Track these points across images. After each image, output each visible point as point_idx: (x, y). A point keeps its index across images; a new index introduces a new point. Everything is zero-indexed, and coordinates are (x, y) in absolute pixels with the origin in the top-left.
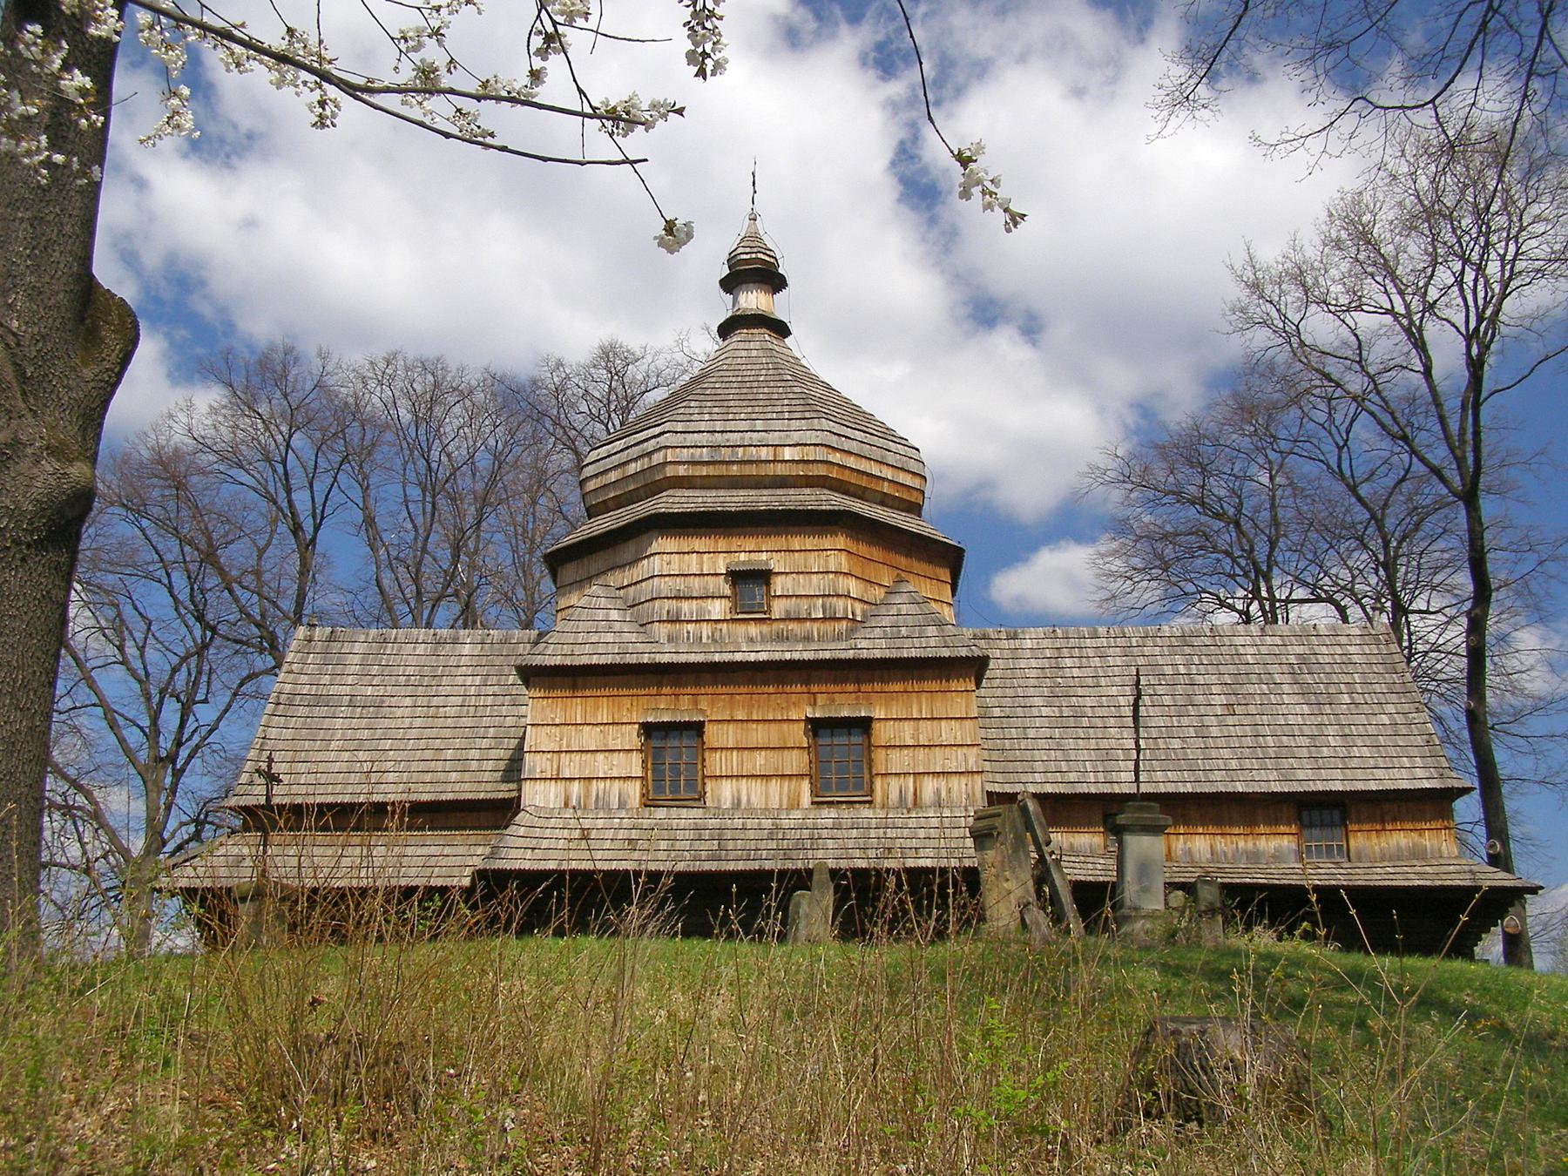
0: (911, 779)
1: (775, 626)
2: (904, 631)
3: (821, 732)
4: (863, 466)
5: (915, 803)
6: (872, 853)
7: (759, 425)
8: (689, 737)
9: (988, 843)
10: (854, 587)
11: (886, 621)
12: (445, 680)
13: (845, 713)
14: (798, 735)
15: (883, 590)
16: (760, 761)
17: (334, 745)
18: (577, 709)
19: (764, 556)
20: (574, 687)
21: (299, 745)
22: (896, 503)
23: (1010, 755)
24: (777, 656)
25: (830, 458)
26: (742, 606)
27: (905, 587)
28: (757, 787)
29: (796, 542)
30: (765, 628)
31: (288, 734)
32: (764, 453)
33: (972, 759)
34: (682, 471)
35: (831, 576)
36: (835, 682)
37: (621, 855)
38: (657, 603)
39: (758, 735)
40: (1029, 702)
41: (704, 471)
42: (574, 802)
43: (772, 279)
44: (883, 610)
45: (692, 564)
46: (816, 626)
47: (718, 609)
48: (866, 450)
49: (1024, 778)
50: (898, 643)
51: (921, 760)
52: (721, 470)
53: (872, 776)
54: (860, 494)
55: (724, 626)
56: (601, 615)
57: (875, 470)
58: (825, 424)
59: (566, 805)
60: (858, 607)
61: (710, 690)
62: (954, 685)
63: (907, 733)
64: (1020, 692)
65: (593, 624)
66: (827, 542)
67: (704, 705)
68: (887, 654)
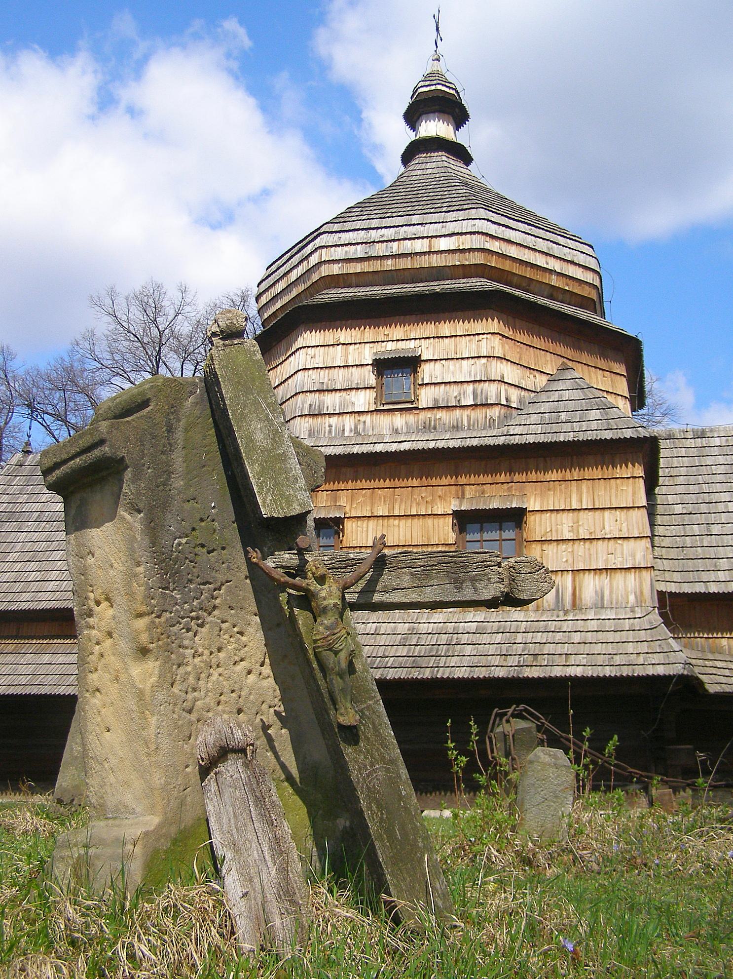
1: (423, 416)
3: (469, 526)
6: (513, 661)
7: (415, 219)
9: (98, 500)
10: (511, 374)
13: (494, 505)
15: (545, 378)
17: (11, 557)
19: (412, 344)
23: (691, 553)
24: (420, 446)
25: (488, 246)
27: (569, 374)
29: (446, 328)
30: (411, 418)
32: (420, 246)
33: (639, 553)
34: (336, 269)
35: (484, 361)
36: (486, 473)
38: (300, 397)
40: (714, 497)
41: (358, 268)
43: (457, 113)
44: (543, 397)
45: (337, 356)
46: (466, 413)
47: (363, 400)
48: (529, 241)
49: (705, 576)
50: (555, 428)
51: (581, 556)
52: (376, 266)
55: (367, 418)
57: (540, 261)
58: (482, 213)
60: (514, 394)
61: (350, 485)
62: (619, 472)
63: (564, 526)
64: (705, 488)
66: (478, 326)
67: (343, 502)
68: (542, 439)
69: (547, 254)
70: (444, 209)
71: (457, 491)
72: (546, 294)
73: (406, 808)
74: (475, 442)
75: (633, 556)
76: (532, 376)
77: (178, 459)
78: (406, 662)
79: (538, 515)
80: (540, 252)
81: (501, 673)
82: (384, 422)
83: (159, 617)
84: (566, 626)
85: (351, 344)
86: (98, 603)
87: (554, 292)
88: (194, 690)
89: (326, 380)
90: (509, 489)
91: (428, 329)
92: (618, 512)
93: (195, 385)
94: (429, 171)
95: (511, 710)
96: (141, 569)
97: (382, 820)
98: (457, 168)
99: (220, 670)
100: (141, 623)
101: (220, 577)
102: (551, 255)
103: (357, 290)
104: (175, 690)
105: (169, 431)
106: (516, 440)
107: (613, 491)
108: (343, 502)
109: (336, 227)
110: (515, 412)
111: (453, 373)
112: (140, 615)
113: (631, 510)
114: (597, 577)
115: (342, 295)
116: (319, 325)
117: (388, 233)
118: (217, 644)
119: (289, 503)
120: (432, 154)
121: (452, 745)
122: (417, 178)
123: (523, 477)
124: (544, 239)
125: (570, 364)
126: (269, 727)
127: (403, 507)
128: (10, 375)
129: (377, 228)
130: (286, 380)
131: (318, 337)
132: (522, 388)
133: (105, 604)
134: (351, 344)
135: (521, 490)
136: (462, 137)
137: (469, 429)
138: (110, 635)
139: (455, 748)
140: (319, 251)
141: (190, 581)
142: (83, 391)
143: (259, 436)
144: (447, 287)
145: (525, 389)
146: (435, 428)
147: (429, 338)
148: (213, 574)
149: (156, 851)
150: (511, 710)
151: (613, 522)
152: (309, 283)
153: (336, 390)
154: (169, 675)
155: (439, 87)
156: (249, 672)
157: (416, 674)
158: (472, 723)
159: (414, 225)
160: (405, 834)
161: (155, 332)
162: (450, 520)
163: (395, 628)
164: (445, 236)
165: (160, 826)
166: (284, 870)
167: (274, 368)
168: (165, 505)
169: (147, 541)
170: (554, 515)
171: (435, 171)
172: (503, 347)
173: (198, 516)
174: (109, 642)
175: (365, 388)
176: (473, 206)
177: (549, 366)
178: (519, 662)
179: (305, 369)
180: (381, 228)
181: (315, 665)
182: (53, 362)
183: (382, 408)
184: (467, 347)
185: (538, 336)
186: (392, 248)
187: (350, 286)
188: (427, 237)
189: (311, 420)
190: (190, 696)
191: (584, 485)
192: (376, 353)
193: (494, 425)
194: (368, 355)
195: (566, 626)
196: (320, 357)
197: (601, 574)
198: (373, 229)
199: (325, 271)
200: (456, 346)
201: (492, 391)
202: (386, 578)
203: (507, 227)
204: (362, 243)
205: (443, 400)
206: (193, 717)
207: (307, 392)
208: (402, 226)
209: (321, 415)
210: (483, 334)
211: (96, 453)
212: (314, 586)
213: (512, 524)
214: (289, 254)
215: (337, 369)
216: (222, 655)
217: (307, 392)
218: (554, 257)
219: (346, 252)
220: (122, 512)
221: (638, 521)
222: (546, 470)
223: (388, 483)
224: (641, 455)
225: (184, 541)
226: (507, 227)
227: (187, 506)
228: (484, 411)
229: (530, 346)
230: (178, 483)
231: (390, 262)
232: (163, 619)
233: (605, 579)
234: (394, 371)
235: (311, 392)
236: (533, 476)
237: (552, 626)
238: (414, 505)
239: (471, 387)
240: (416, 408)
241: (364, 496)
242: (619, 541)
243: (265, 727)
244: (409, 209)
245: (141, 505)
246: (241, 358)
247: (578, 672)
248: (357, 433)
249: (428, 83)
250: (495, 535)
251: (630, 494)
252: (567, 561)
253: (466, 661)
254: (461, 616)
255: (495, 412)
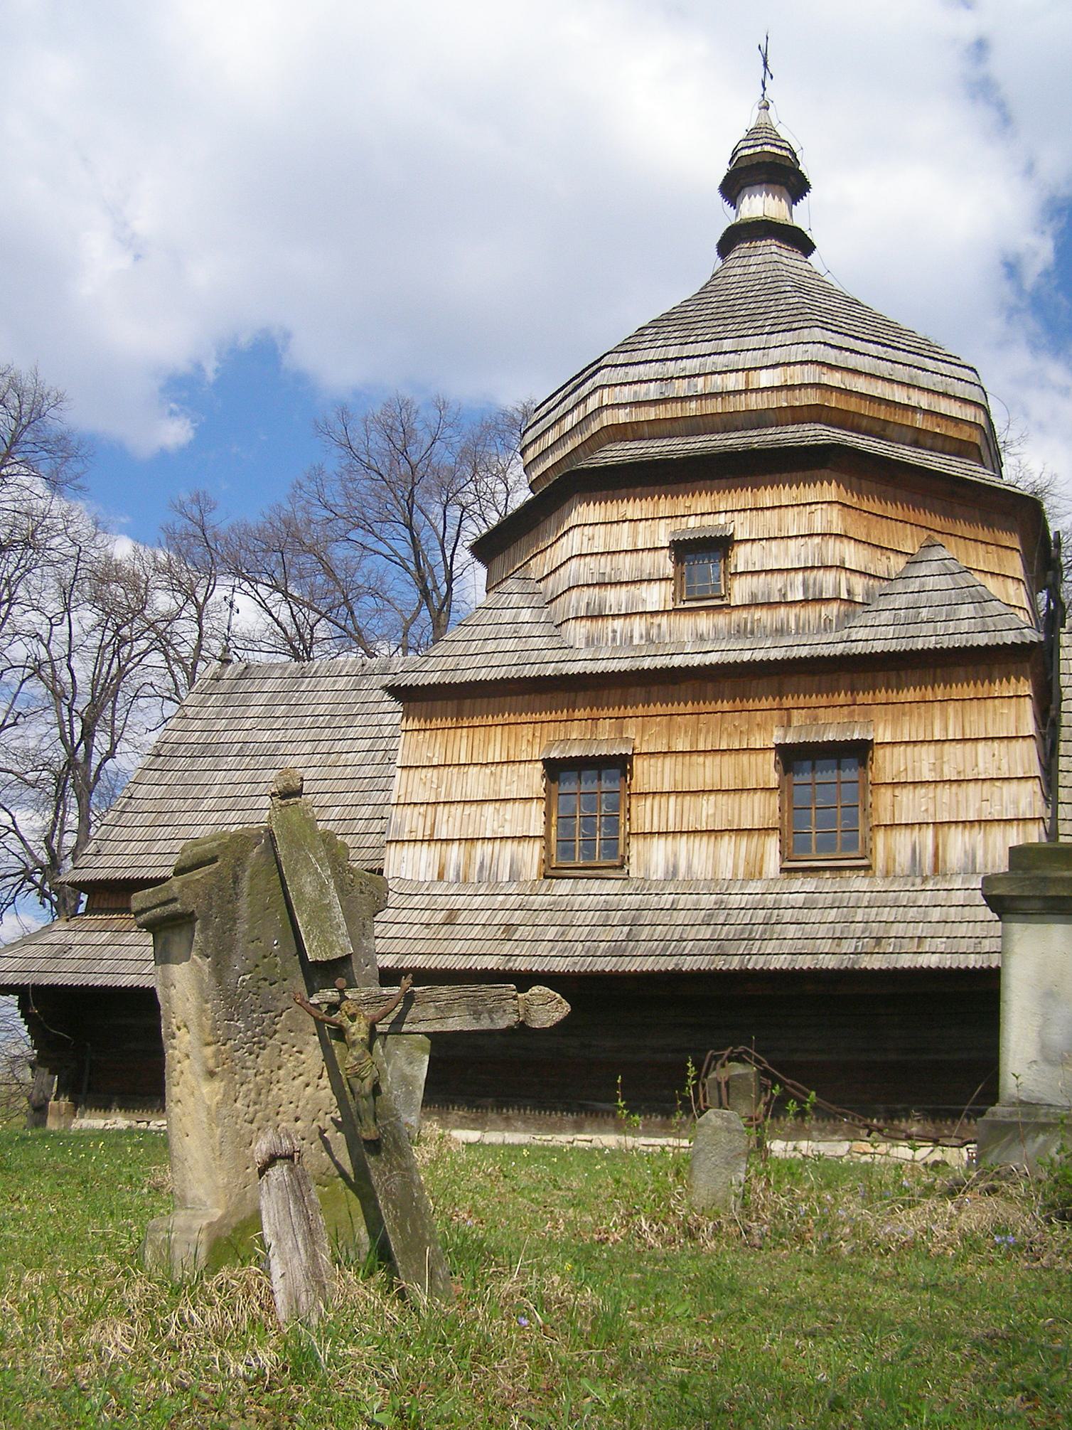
0: (930, 831)
1: (737, 616)
2: (924, 613)
4: (879, 389)
5: (936, 869)
6: (848, 946)
7: (727, 345)
8: (612, 780)
10: (853, 555)
11: (901, 601)
12: (359, 720)
13: (829, 737)
14: (767, 770)
15: (902, 561)
16: (707, 811)
17: (206, 804)
18: (461, 744)
19: (722, 519)
20: (459, 715)
21: (167, 805)
22: (939, 443)
24: (731, 657)
25: (825, 380)
26: (690, 590)
27: (937, 553)
28: (702, 846)
29: (767, 496)
30: (721, 620)
31: (158, 791)
32: (733, 382)
34: (622, 416)
35: (817, 540)
36: (819, 692)
37: (488, 946)
38: (575, 592)
39: (707, 772)
41: (651, 413)
42: (451, 875)
44: (899, 586)
45: (623, 536)
46: (794, 611)
47: (656, 596)
48: (884, 368)
50: (912, 629)
51: (946, 803)
52: (674, 411)
53: (546, 837)
54: (880, 430)
55: (663, 620)
56: (508, 615)
57: (899, 395)
58: (818, 334)
59: (441, 876)
60: (859, 584)
61: (640, 710)
62: (997, 689)
63: (924, 763)
65: (495, 630)
66: (809, 493)
67: (631, 732)
68: (893, 646)
69: (909, 386)
70: (767, 329)
71: (781, 718)
72: (908, 441)
73: (417, 1207)
74: (804, 652)
75: (1016, 803)
76: (884, 558)
77: (243, 906)
78: (709, 948)
79: (888, 749)
80: (899, 383)
81: (830, 963)
82: (685, 624)
83: (224, 1045)
84: (923, 899)
85: (641, 520)
86: (179, 1029)
87: (919, 439)
88: (255, 1103)
89: (608, 570)
90: (851, 714)
91: (744, 498)
92: (996, 744)
93: (261, 836)
94: (753, 269)
95: (727, 1053)
96: (209, 1006)
97: (396, 1217)
98: (791, 262)
99: (280, 1085)
100: (209, 1050)
101: (281, 1005)
102: (914, 387)
103: (650, 443)
104: (238, 1105)
105: (234, 882)
106: (859, 648)
107: (990, 715)
108: (631, 732)
109: (622, 358)
110: (859, 609)
111: (776, 557)
112: (208, 1044)
113: (1014, 741)
114: (967, 832)
115: (631, 452)
116: (599, 494)
117: (691, 366)
118: (277, 1064)
119: (332, 948)
120: (758, 243)
121: (621, 1104)
122: (735, 279)
123: (869, 698)
124: (904, 365)
125: (938, 538)
126: (325, 1131)
127: (709, 740)
128: (208, 533)
129: (677, 359)
130: (557, 569)
131: (597, 512)
132: (870, 575)
133: (184, 1030)
134: (641, 520)
135: (866, 715)
136: (802, 216)
137: (797, 633)
138: (187, 1056)
139: (625, 1107)
140: (600, 391)
141: (253, 1011)
142: (310, 550)
143: (308, 889)
144: (770, 438)
145: (875, 577)
146: (752, 632)
147: (744, 510)
148: (275, 1003)
149: (218, 1239)
150: (727, 1053)
151: (989, 756)
152: (587, 435)
153: (621, 583)
154: (232, 1093)
155: (767, 148)
156: (307, 1085)
157: (720, 964)
158: (689, 1065)
159: (726, 353)
160: (415, 1230)
161: (405, 468)
162: (772, 756)
163: (698, 901)
164: (767, 367)
165: (223, 1217)
166: (314, 1257)
167: (542, 552)
168: (229, 949)
169: (214, 981)
170: (910, 748)
171: (761, 268)
172: (844, 520)
173: (261, 954)
174: (187, 1061)
175: (660, 580)
176: (806, 324)
177: (909, 542)
178: (856, 947)
179: (581, 555)
180: (682, 358)
181: (347, 1089)
182: (267, 512)
183: (682, 606)
184: (794, 522)
185: (894, 502)
186: (696, 386)
187: (641, 439)
188: (743, 370)
189: (589, 623)
190: (251, 1109)
191: (951, 708)
192: (674, 533)
193: (831, 628)
194: (663, 534)
195: (923, 899)
196: (601, 539)
197: (972, 827)
198: (671, 359)
199: (608, 418)
200: (780, 520)
201: (828, 582)
202: (414, 1011)
203: (852, 351)
204: (656, 380)
205: (763, 594)
206: (254, 1126)
207: (583, 586)
208: (709, 355)
209: (602, 616)
210: (817, 503)
211: (171, 908)
212: (347, 1023)
213: (854, 761)
214: (561, 394)
215: (622, 555)
216: (281, 1072)
217: (583, 586)
218: (920, 388)
219: (635, 392)
220: (194, 956)
221: (1025, 757)
222: (899, 688)
223: (690, 708)
224: (1028, 665)
225: (247, 977)
226: (852, 351)
227: (251, 946)
228: (817, 608)
229: (882, 517)
230: (243, 927)
231: (693, 405)
232: (228, 1046)
233: (977, 835)
234: (699, 556)
235: (588, 585)
236: (882, 696)
237: (904, 898)
238: (725, 736)
239: (800, 576)
240: (728, 606)
241: (659, 724)
242: (998, 784)
243: (322, 1132)
244: (720, 329)
245: (209, 951)
246: (295, 818)
247: (931, 961)
248: (650, 640)
249: (751, 143)
250: (831, 776)
251: (1013, 718)
252: (927, 810)
253: (787, 946)
254: (785, 885)
255: (833, 610)
